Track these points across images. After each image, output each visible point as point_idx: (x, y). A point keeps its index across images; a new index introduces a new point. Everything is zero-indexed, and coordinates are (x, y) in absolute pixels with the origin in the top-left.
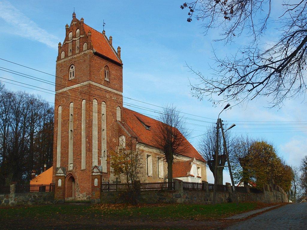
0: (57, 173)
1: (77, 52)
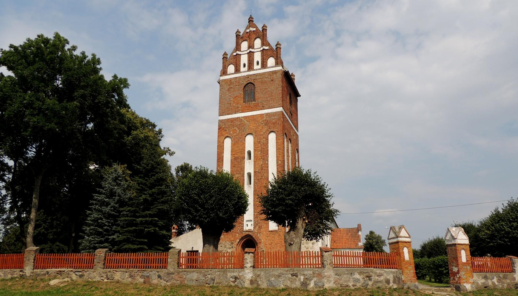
0: (401, 237)
1: (256, 67)
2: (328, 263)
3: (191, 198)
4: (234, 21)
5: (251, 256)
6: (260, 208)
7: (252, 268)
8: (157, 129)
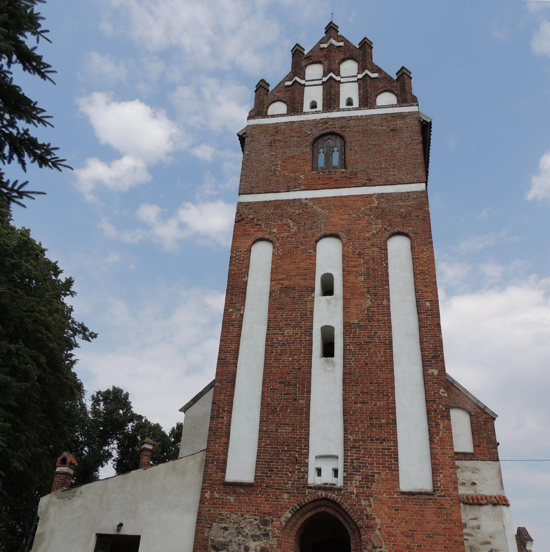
8: (62, 278)
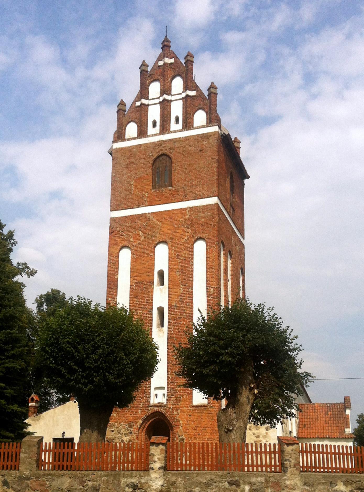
1: (174, 126)
2: (292, 464)
3: (61, 350)
4: (136, 48)
5: (161, 450)
6: (177, 368)
7: (162, 471)
